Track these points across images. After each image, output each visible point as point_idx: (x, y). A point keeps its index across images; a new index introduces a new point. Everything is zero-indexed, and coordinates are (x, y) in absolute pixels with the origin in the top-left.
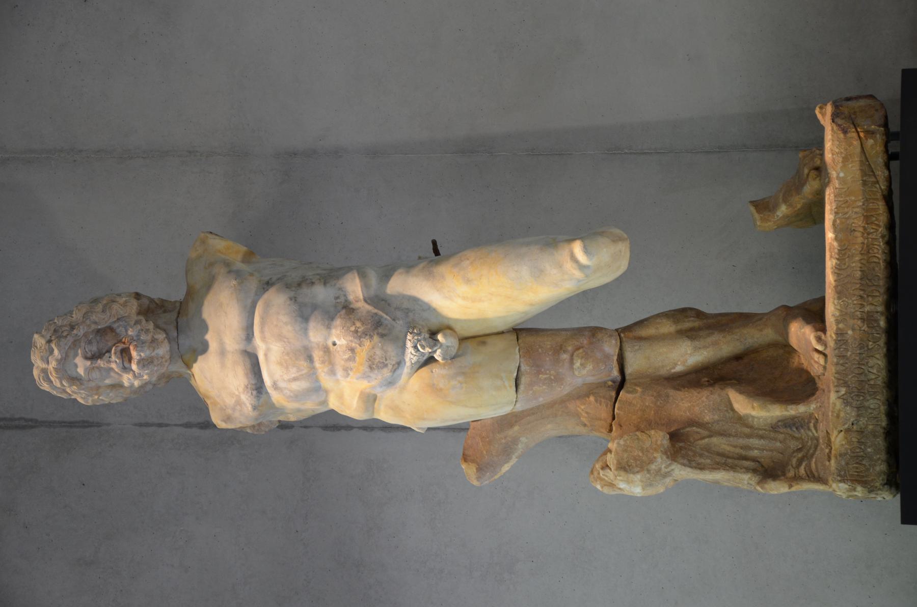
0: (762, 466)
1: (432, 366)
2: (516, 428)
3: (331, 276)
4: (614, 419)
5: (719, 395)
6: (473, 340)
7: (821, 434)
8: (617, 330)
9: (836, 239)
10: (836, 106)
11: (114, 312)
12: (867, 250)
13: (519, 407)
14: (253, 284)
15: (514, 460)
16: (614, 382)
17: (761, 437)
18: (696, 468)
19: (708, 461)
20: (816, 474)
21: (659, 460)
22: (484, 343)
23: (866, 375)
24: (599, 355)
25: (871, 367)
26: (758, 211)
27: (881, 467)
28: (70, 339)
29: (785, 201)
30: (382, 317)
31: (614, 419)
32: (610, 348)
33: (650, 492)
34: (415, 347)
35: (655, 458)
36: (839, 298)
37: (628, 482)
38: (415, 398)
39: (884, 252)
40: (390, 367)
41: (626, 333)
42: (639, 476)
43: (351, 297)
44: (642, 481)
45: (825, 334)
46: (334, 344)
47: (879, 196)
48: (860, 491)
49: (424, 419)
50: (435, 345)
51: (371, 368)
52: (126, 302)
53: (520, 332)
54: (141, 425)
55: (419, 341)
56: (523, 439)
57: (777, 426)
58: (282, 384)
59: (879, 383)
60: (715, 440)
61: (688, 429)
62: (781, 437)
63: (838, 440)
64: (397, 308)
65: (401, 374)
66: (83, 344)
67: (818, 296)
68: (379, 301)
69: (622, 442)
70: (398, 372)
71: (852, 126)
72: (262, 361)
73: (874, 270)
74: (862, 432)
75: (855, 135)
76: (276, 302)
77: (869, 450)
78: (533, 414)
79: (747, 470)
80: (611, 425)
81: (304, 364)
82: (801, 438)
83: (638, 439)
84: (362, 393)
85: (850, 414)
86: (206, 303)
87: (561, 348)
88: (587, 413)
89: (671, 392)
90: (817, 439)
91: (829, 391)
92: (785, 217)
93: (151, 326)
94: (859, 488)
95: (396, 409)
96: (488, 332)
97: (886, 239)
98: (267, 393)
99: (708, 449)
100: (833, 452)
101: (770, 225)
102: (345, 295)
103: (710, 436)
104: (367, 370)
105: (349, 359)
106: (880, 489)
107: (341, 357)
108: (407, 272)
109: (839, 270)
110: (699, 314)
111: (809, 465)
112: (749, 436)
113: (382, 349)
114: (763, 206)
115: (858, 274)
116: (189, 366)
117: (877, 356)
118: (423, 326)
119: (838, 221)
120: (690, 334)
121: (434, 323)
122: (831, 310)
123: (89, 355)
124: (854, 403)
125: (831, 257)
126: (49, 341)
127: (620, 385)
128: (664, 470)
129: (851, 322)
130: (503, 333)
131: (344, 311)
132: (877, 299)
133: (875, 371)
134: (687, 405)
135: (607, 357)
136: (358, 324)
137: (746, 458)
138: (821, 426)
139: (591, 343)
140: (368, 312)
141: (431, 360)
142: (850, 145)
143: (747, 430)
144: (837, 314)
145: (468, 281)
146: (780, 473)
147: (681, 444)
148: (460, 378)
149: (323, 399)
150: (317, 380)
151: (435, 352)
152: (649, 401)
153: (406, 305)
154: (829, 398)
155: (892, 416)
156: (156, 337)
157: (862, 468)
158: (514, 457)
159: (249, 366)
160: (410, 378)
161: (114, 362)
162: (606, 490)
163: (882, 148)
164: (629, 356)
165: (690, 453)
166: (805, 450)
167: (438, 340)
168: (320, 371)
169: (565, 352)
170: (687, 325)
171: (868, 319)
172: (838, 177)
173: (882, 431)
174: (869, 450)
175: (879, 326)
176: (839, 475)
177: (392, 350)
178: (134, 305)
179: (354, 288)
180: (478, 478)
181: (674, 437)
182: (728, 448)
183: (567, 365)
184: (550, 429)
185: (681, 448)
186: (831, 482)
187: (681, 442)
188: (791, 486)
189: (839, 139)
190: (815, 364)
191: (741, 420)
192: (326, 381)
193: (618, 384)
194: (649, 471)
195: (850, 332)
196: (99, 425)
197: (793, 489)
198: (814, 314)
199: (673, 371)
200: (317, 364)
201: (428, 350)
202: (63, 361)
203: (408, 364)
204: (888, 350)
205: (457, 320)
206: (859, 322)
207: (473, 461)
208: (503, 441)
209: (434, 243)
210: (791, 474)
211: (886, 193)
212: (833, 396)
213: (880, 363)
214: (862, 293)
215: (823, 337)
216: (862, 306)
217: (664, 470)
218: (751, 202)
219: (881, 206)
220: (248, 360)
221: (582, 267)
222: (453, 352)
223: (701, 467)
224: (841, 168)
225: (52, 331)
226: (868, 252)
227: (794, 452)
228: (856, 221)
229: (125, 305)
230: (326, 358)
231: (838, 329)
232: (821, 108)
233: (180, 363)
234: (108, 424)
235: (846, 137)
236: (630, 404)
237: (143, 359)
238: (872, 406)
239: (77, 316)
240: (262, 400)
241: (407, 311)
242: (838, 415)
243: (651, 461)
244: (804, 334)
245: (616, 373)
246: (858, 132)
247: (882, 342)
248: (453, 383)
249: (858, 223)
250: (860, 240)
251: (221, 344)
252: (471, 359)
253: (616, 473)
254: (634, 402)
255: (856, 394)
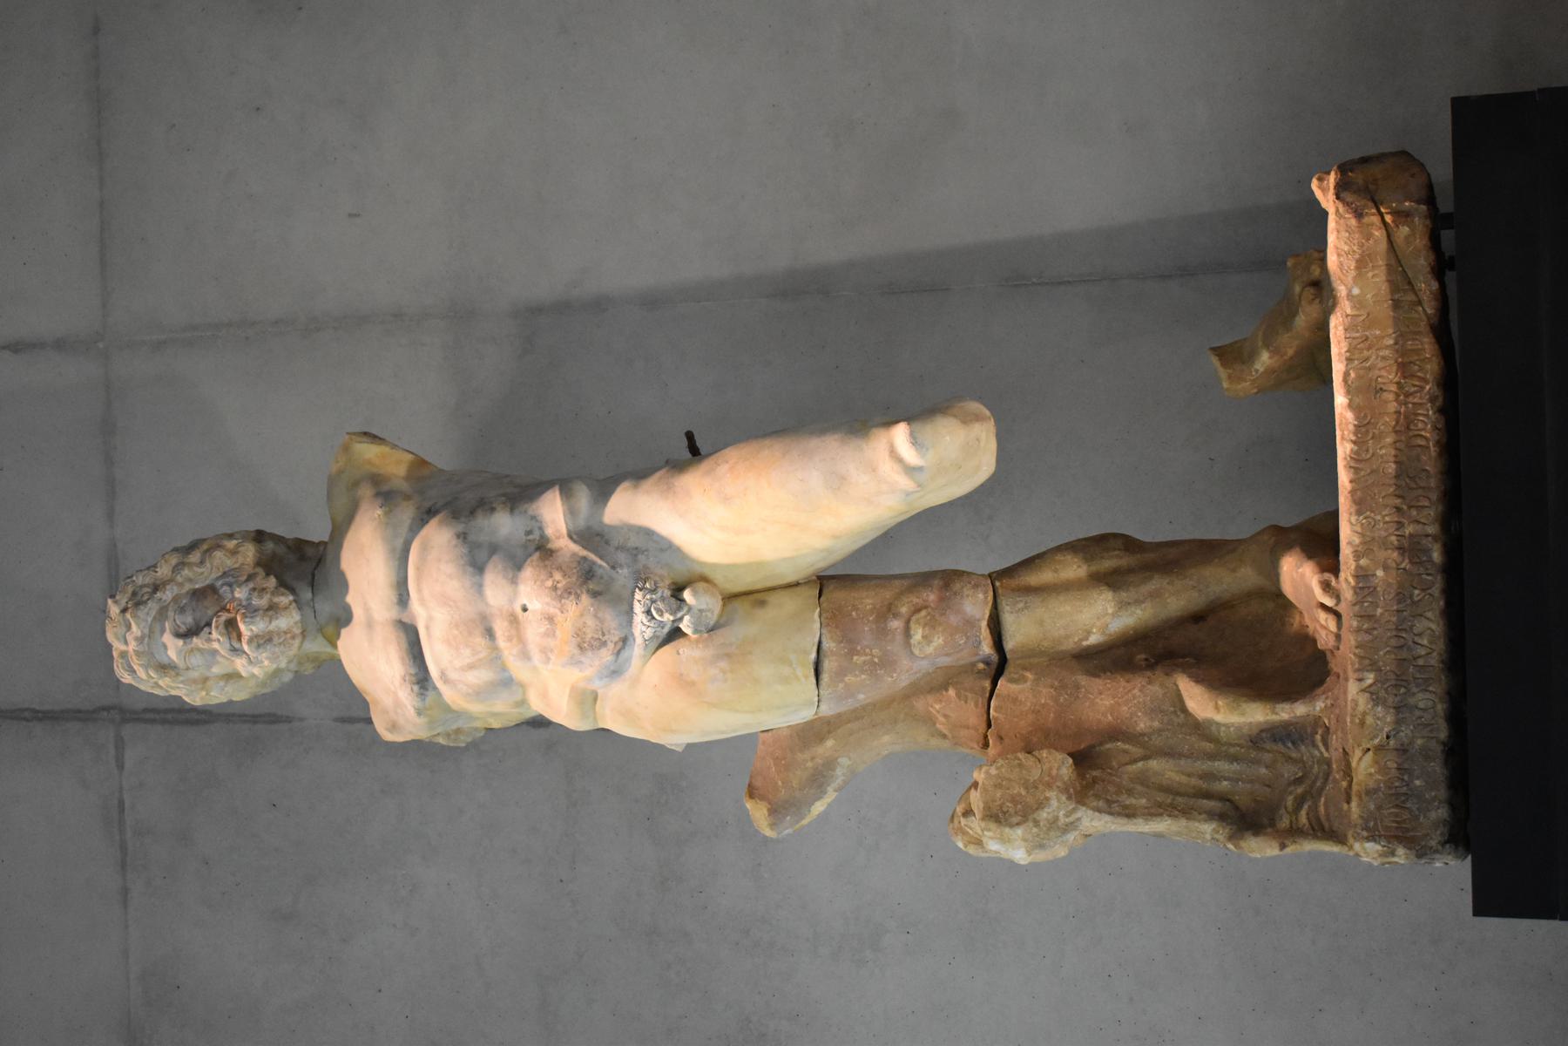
0: (1237, 808)
1: (678, 644)
2: (830, 743)
3: (521, 494)
4: (989, 726)
5: (1162, 685)
6: (747, 597)
7: (1335, 755)
8: (990, 576)
9: (1350, 406)
10: (1343, 169)
11: (216, 562)
12: (1405, 424)
13: (827, 710)
14: (406, 513)
15: (831, 795)
16: (987, 663)
17: (1234, 759)
18: (1119, 814)
19: (1143, 801)
20: (1326, 825)
21: (1054, 803)
22: (762, 603)
23: (1410, 649)
24: (953, 619)
25: (1420, 635)
26: (1224, 364)
27: (1441, 813)
28: (152, 607)
29: (1267, 346)
30: (594, 563)
31: (989, 726)
32: (975, 606)
33: (1041, 856)
34: (648, 612)
35: (1047, 799)
36: (1359, 513)
37: (1004, 840)
38: (658, 697)
39: (1435, 428)
40: (611, 646)
41: (1005, 580)
42: (1019, 831)
43: (549, 532)
44: (1025, 840)
45: (1337, 576)
46: (525, 609)
47: (1423, 326)
48: (1402, 856)
49: (672, 731)
50: (679, 609)
51: (581, 648)
52: (238, 546)
53: (828, 583)
54: (343, 720)
55: (653, 601)
56: (844, 761)
57: (1261, 738)
58: (453, 675)
59: (1433, 662)
60: (1154, 764)
61: (1108, 746)
62: (1267, 757)
63: (1364, 767)
64: (619, 548)
65: (629, 660)
66: (171, 614)
67: (1318, 510)
68: (591, 536)
69: (993, 771)
70: (625, 654)
71: (1370, 204)
72: (448, 637)
73: (1419, 460)
74: (1405, 751)
75: (1376, 219)
76: (438, 538)
77: (1418, 783)
78: (857, 719)
79: (1212, 816)
80: (986, 737)
81: (480, 641)
82: (1302, 761)
83: (1020, 765)
84: (573, 688)
85: (1382, 719)
86: (346, 545)
87: (889, 609)
88: (945, 716)
89: (1083, 680)
90: (1328, 763)
91: (1347, 680)
92: (1269, 371)
93: (272, 582)
94: (1401, 851)
95: (627, 715)
96: (769, 584)
97: (1439, 403)
98: (435, 688)
99: (1143, 780)
100: (1355, 787)
101: (1245, 387)
102: (541, 528)
103: (1145, 758)
104: (576, 651)
105: (547, 635)
106: (1437, 851)
107: (534, 631)
108: (636, 487)
109: (1357, 461)
110: (1129, 544)
111: (1314, 809)
112: (1212, 757)
113: (595, 616)
114: (1233, 355)
115: (1391, 468)
116: (335, 646)
117: (1429, 614)
118: (662, 578)
119: (1353, 375)
120: (1111, 580)
121: (681, 572)
122: (1348, 532)
123: (183, 629)
124: (1390, 699)
125: (1343, 438)
126: (124, 611)
127: (999, 666)
128: (1063, 820)
129: (1382, 555)
130: (797, 584)
131: (537, 554)
132: (1426, 512)
133: (1425, 642)
134: (1106, 702)
135: (970, 623)
136: (558, 576)
137: (1208, 795)
138: (1334, 740)
139: (941, 599)
140: (574, 554)
141: (675, 634)
142: (1368, 237)
143: (1209, 746)
144: (1357, 540)
145: (726, 500)
146: (1265, 821)
147: (1095, 773)
148: (723, 664)
149: (519, 697)
150: (504, 669)
151: (681, 619)
152: (1045, 695)
153: (634, 542)
154: (1345, 693)
155: (1456, 718)
156: (276, 600)
157: (1406, 816)
158: (830, 789)
159: (405, 645)
160: (644, 664)
161: (216, 639)
162: (972, 850)
163: (1425, 241)
164: (1009, 619)
165: (1111, 788)
166: (1308, 782)
167: (683, 600)
168: (506, 653)
169: (896, 616)
170: (1108, 564)
171: (1411, 549)
172: (1350, 296)
173: (1439, 748)
174: (1418, 783)
175: (1430, 560)
176: (1366, 829)
177: (611, 619)
178: (249, 552)
179: (553, 514)
180: (772, 826)
181: (1083, 759)
182: (1177, 778)
183: (899, 638)
184: (886, 743)
185: (1095, 781)
186: (1351, 841)
187: (1093, 765)
188: (1283, 846)
189: (1348, 229)
190: (1323, 628)
191: (1200, 728)
192: (518, 669)
193: (994, 666)
194: (1036, 823)
195: (1380, 573)
196: (289, 720)
197: (1288, 850)
198: (1321, 543)
199: (1085, 643)
200: (501, 643)
201: (668, 617)
202: (149, 637)
203: (639, 640)
204: (1448, 604)
205: (715, 566)
206: (1395, 554)
207: (762, 798)
208: (810, 764)
209: (690, 436)
210: (1284, 823)
211: (1435, 320)
212: (1353, 688)
213: (1433, 626)
214: (1398, 501)
215: (1333, 583)
216: (1400, 525)
217: (1063, 820)
218: (1213, 349)
219: (1427, 346)
220: (402, 635)
221: (910, 470)
222: (712, 619)
223: (1129, 813)
224: (1355, 279)
225: (129, 595)
226: (1408, 428)
227: (1289, 784)
228: (1384, 373)
229: (234, 553)
230: (513, 632)
231: (1358, 567)
232: (1320, 179)
233: (320, 639)
234: (301, 720)
235: (1360, 225)
236: (1015, 700)
237: (257, 636)
238: (1421, 705)
239: (164, 571)
240: (428, 700)
241: (635, 553)
242: (1362, 720)
243: (1040, 805)
244: (1303, 575)
245: (987, 649)
246: (1381, 215)
247: (1436, 590)
248: (713, 671)
249: (1388, 376)
250: (1392, 407)
251: (367, 610)
252: (744, 628)
253: (983, 824)
254: (1022, 698)
255: (1395, 686)
